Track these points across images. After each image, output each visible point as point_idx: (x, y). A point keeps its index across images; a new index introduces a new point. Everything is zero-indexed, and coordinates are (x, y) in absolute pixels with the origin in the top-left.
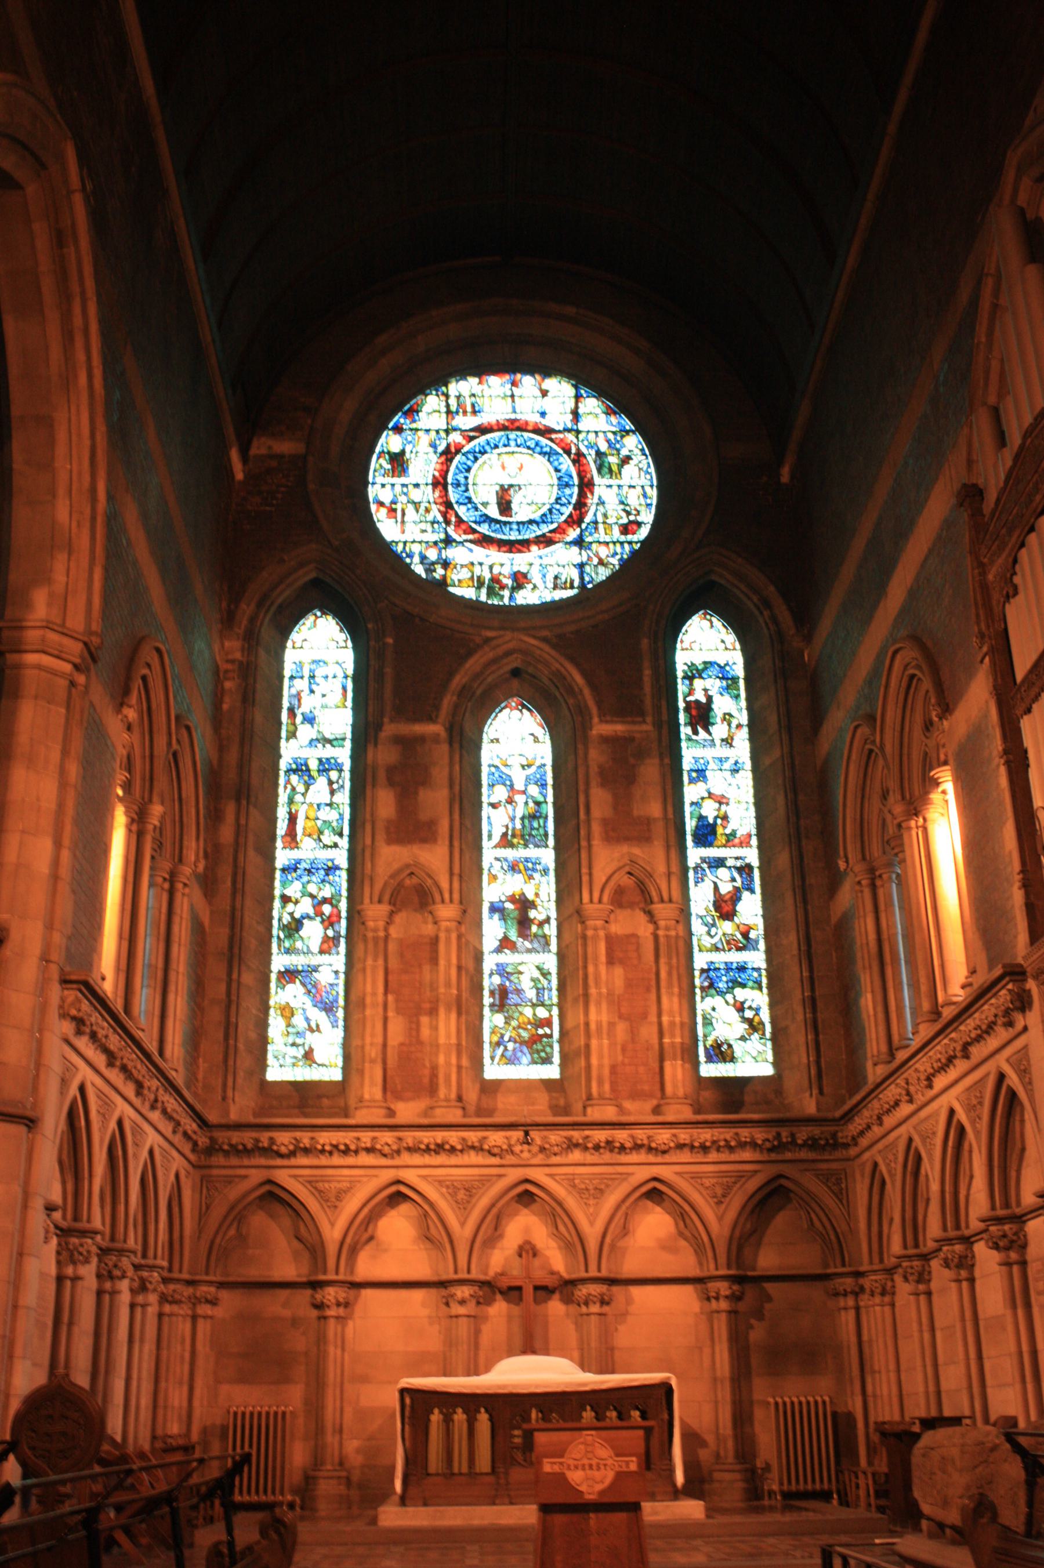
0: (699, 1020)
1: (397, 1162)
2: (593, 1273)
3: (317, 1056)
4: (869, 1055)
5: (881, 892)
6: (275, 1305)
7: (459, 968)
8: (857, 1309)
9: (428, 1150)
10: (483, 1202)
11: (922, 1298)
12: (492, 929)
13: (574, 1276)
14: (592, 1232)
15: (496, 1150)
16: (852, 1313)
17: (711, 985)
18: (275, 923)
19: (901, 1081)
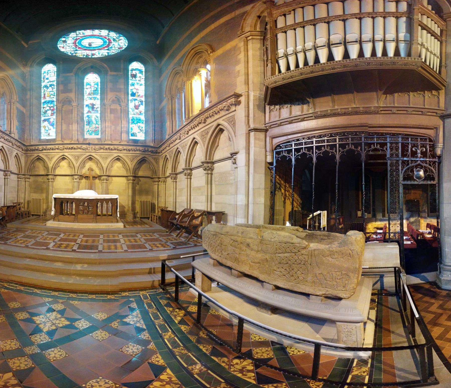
0: (130, 128)
1: (63, 151)
2: (105, 174)
3: (50, 134)
4: (167, 134)
5: (173, 101)
6: (40, 179)
7: (77, 115)
8: (158, 185)
9: (69, 149)
10: (81, 159)
11: (175, 183)
12: (86, 109)
13: (101, 175)
14: (105, 166)
15: (84, 149)
16: (157, 186)
17: (133, 122)
18: (42, 112)
19: (179, 134)
